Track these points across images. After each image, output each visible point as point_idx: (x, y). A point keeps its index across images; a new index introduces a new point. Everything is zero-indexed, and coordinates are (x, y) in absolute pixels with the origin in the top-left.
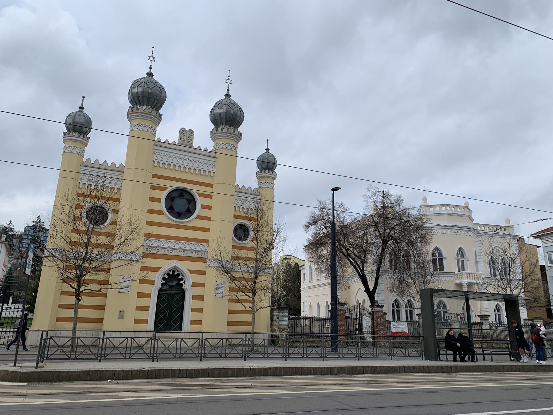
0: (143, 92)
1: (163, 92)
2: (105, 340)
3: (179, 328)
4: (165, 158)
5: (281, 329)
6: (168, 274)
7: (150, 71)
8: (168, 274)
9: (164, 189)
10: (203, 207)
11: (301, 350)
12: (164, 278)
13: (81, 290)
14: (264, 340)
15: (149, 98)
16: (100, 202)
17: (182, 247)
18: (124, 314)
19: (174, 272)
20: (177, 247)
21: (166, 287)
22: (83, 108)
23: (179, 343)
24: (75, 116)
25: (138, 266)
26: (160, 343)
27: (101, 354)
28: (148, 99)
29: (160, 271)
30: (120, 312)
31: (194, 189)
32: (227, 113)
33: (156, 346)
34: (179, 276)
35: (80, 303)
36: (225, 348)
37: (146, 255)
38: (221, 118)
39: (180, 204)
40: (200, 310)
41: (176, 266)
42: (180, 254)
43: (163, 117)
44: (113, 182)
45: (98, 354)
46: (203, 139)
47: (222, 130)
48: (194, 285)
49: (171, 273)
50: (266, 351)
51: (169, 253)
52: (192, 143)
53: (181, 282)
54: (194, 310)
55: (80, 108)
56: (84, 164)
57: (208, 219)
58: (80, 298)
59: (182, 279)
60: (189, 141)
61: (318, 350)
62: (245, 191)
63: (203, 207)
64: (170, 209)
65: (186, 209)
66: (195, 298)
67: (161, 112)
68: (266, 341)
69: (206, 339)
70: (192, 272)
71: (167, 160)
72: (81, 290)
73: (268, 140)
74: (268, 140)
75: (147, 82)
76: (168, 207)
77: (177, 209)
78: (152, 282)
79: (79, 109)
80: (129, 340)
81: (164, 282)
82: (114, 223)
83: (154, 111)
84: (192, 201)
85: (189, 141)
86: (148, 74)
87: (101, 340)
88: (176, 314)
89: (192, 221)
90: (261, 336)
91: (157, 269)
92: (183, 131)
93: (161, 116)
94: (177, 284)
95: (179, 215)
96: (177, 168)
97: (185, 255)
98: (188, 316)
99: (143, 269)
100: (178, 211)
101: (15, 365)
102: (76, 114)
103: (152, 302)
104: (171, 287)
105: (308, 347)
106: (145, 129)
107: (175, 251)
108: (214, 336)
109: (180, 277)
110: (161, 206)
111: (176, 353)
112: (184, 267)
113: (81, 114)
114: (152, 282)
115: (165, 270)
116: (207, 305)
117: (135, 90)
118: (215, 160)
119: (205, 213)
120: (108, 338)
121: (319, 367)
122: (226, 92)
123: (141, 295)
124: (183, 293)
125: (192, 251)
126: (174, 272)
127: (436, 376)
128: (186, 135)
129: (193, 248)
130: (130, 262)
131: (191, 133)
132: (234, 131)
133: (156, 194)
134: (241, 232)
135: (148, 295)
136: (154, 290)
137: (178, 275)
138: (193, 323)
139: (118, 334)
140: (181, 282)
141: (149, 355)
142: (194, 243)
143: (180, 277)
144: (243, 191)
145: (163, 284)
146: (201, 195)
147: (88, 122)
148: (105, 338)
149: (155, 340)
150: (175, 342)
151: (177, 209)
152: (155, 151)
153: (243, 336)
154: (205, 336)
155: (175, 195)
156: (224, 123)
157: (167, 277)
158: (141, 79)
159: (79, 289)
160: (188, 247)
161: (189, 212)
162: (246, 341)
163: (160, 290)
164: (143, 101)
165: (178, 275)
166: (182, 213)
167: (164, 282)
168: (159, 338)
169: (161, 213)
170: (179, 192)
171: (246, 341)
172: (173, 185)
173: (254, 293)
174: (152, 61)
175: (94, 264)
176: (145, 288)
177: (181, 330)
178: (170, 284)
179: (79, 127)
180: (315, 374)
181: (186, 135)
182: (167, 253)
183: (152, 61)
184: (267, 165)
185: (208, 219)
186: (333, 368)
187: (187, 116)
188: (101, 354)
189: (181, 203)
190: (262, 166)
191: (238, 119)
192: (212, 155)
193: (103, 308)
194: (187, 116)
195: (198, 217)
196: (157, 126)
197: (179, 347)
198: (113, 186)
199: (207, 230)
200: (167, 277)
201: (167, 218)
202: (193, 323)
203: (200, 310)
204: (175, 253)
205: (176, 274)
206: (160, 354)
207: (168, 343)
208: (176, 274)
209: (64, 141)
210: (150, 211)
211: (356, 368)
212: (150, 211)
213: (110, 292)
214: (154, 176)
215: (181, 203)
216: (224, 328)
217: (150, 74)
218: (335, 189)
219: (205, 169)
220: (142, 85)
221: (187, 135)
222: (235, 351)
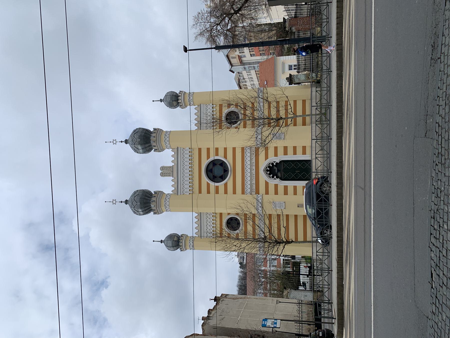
1: (137, 131)
3: (309, 161)
6: (270, 174)
8: (270, 174)
9: (208, 185)
11: (324, 58)
12: (273, 177)
14: (316, 91)
15: (145, 203)
16: (223, 119)
17: (249, 167)
19: (267, 171)
20: (249, 171)
21: (279, 174)
22: (162, 240)
25: (265, 197)
28: (145, 202)
29: (268, 181)
30: (298, 207)
31: (205, 163)
35: (294, 240)
36: (324, 139)
37: (257, 192)
39: (218, 171)
40: (295, 148)
42: (254, 168)
43: (156, 127)
44: (209, 224)
46: (166, 157)
47: (154, 137)
48: (276, 155)
49: (269, 172)
50: (325, 20)
51: (255, 176)
52: (170, 167)
53: (275, 164)
54: (295, 153)
55: (161, 243)
56: (200, 236)
57: (225, 149)
59: (272, 164)
61: (324, 24)
63: (217, 188)
64: (222, 178)
66: (286, 153)
67: (152, 130)
68: (317, 89)
70: (267, 158)
73: (153, 101)
74: (153, 101)
75: (133, 207)
76: (221, 179)
77: (222, 173)
78: (276, 186)
79: (163, 243)
80: (318, 254)
81: (275, 177)
82: (237, 105)
84: (214, 163)
86: (126, 204)
88: (298, 165)
89: (229, 162)
90: (314, 93)
91: (267, 184)
92: (162, 175)
93: (155, 129)
95: (226, 171)
96: (191, 188)
97: (254, 164)
98: (300, 157)
99: (267, 193)
101: (334, 323)
103: (290, 184)
104: (278, 171)
105: (322, 52)
109: (271, 166)
112: (263, 164)
113: (165, 242)
114: (276, 186)
117: (141, 151)
118: (179, 149)
119: (221, 152)
120: (316, 137)
121: (337, 196)
123: (286, 193)
124: (282, 162)
125: (251, 159)
126: (267, 171)
127: (346, 279)
128: (165, 172)
129: (249, 159)
131: (162, 168)
132: (155, 197)
133: (212, 189)
134: (232, 119)
135: (286, 188)
137: (269, 167)
138: (304, 153)
140: (275, 164)
142: (245, 174)
143: (271, 166)
145: (277, 178)
146: (208, 157)
147: (171, 237)
149: (317, 172)
150: (319, 159)
151: (222, 173)
154: (314, 104)
155: (211, 175)
156: (149, 145)
157: (272, 175)
160: (249, 163)
161: (222, 164)
162: (317, 106)
163: (282, 179)
164: (147, 206)
165: (269, 167)
167: (275, 177)
169: (226, 185)
171: (317, 106)
172: (205, 179)
173: (279, 119)
174: (116, 142)
175: (267, 234)
176: (281, 190)
177: (310, 161)
178: (276, 171)
179: (175, 242)
180: (342, 291)
181: (165, 172)
183: (116, 142)
185: (225, 149)
186: (337, 116)
187: (150, 171)
189: (217, 171)
191: (143, 134)
193: (296, 216)
194: (150, 171)
195: (225, 157)
196: (164, 193)
197: (322, 156)
198: (212, 227)
199: (234, 149)
200: (272, 175)
201: (229, 180)
202: (304, 153)
203: (295, 148)
204: (254, 172)
205: (269, 169)
208: (269, 169)
210: (226, 192)
211: (338, 143)
212: (226, 192)
213: (285, 213)
214: (200, 192)
215: (217, 171)
216: (308, 128)
217: (126, 142)
218: (186, 50)
219: (188, 156)
220: (136, 146)
221: (165, 171)
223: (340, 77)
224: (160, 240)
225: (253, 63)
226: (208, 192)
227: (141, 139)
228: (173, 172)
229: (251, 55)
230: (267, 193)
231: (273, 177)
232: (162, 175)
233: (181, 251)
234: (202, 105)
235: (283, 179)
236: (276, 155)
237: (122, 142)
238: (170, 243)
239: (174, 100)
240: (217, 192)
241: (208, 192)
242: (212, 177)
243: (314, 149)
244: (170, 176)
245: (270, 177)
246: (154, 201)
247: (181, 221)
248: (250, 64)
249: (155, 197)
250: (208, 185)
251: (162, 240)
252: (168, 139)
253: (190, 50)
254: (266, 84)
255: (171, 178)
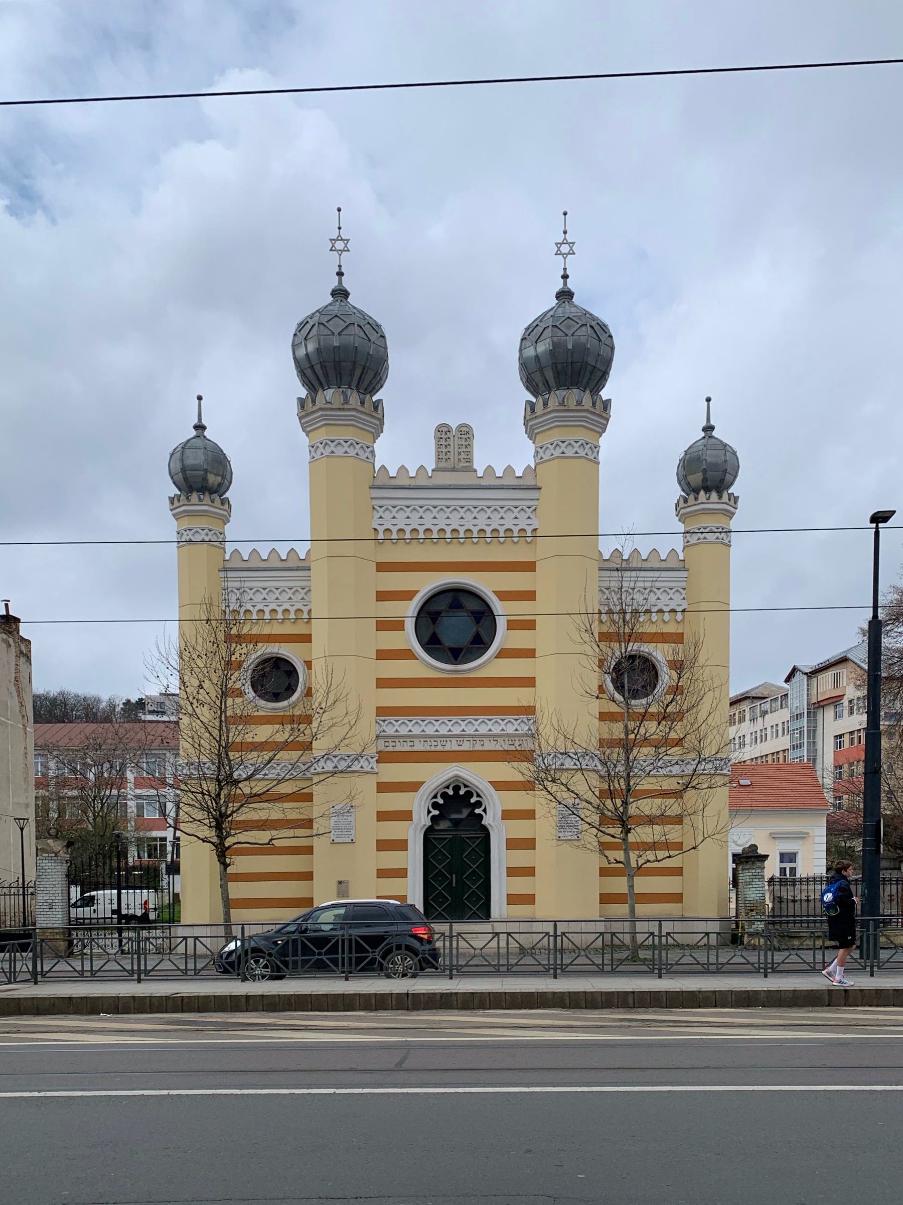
0: (318, 350)
2: (559, 939)
3: (484, 911)
4: (401, 516)
5: (756, 907)
6: (444, 795)
7: (340, 282)
8: (444, 795)
9: (408, 595)
10: (512, 625)
12: (435, 806)
13: (227, 845)
14: (707, 934)
15: (337, 366)
17: (470, 730)
18: (347, 887)
19: (457, 788)
20: (457, 730)
21: (443, 825)
23: (503, 944)
24: (183, 453)
25: (372, 781)
26: (462, 944)
27: (766, 963)
28: (342, 365)
30: (340, 882)
32: (555, 351)
33: (454, 951)
34: (472, 796)
35: (230, 870)
37: (384, 757)
38: (541, 370)
39: (456, 629)
41: (456, 776)
42: (466, 746)
45: (549, 965)
46: (505, 446)
48: (508, 815)
49: (451, 792)
51: (439, 748)
52: (470, 460)
53: (477, 811)
54: (512, 872)
55: (196, 427)
57: (530, 653)
58: (228, 861)
59: (479, 804)
60: (463, 456)
62: (657, 565)
65: (469, 636)
66: (512, 844)
67: (605, 394)
68: (713, 937)
69: (563, 934)
70: (499, 786)
71: (408, 521)
72: (227, 845)
73: (708, 400)
74: (708, 400)
75: (324, 320)
76: (426, 639)
77: (448, 641)
78: (407, 816)
79: (194, 433)
81: (436, 812)
83: (354, 398)
85: (463, 456)
87: (552, 939)
89: (486, 665)
90: (701, 927)
91: (414, 787)
92: (443, 431)
94: (468, 816)
95: (456, 655)
97: (478, 747)
99: (383, 787)
100: (452, 645)
102: (185, 446)
103: (413, 859)
104: (456, 823)
106: (340, 451)
107: (454, 740)
108: (584, 927)
109: (473, 800)
110: (409, 638)
111: (603, 964)
112: (478, 776)
113: (198, 442)
114: (407, 816)
115: (433, 787)
116: (542, 857)
121: (375, 995)
122: (560, 285)
125: (495, 737)
126: (457, 788)
128: (454, 443)
129: (496, 730)
130: (322, 777)
133: (392, 609)
134: (633, 675)
136: (413, 834)
138: (513, 899)
139: (584, 927)
140: (477, 811)
141: (756, 966)
142: (445, 719)
143: (473, 800)
144: (634, 565)
145: (434, 818)
148: (559, 933)
150: (494, 944)
151: (448, 641)
152: (375, 502)
153: (550, 928)
155: (442, 605)
157: (441, 801)
158: (311, 317)
159: (222, 843)
160: (483, 730)
162: (660, 937)
164: (326, 375)
165: (469, 794)
166: (460, 650)
167: (436, 812)
168: (459, 934)
169: (408, 654)
170: (450, 595)
171: (660, 937)
173: (623, 824)
174: (565, 255)
176: (393, 830)
178: (454, 816)
179: (202, 477)
180: (116, 1011)
181: (454, 443)
182: (433, 749)
184: (708, 475)
185: (530, 653)
187: (456, 384)
188: (766, 963)
189: (456, 625)
190: (689, 484)
191: (591, 361)
192: (526, 486)
194: (456, 384)
195: (503, 654)
200: (441, 801)
201: (426, 665)
202: (513, 899)
204: (452, 746)
205: (462, 792)
206: (567, 966)
207: (478, 943)
208: (462, 792)
209: (177, 516)
210: (382, 655)
211: (543, 995)
212: (382, 655)
215: (456, 625)
216: (593, 910)
217: (565, 295)
218: (880, 518)
221: (454, 443)
222: (794, 958)
223: (747, 1000)
224: (204, 422)
225: (813, 744)
226: (382, 596)
227: (572, 351)
228: (454, 470)
229: (841, 736)
230: (383, 787)
231: (435, 806)
232: (443, 431)
233: (172, 500)
234: (685, 574)
235: (428, 834)
236: (508, 815)
237: (565, 277)
238: (196, 459)
239: (708, 475)
240: (384, 625)
241: (382, 596)
242: (434, 607)
243: (524, 927)
244: (439, 459)
245: (435, 797)
246: (346, 401)
247: (278, 494)
248: (812, 732)
249: (363, 403)
250: (408, 595)
251: (204, 428)
252: (570, 452)
253: (877, 534)
254: (742, 782)
255: (430, 466)
